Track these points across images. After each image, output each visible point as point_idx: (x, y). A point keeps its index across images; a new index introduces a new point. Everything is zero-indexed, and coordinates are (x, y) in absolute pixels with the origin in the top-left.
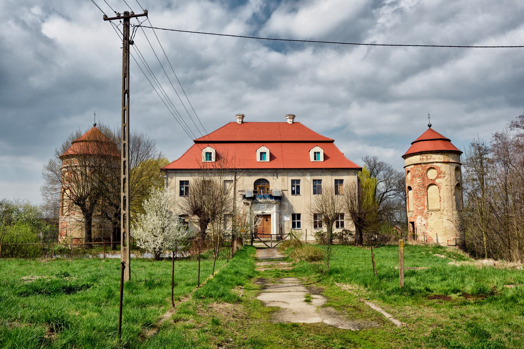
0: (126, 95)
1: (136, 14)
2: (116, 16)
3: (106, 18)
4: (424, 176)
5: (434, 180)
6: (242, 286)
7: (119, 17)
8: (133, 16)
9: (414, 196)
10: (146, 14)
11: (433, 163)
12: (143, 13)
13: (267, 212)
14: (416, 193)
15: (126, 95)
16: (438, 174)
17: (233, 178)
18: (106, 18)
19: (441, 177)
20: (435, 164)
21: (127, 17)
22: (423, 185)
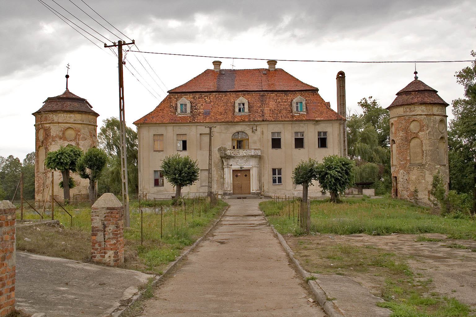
0: (122, 100)
1: (127, 42)
2: (113, 45)
3: (106, 46)
4: (406, 130)
5: (417, 134)
6: (128, 139)
7: (115, 45)
8: (125, 44)
9: (397, 150)
10: (133, 43)
11: (417, 115)
12: (131, 42)
13: (246, 167)
14: (399, 147)
15: (122, 100)
16: (421, 128)
17: (207, 131)
18: (106, 46)
19: (423, 130)
20: (418, 117)
21: (120, 45)
22: (406, 138)
